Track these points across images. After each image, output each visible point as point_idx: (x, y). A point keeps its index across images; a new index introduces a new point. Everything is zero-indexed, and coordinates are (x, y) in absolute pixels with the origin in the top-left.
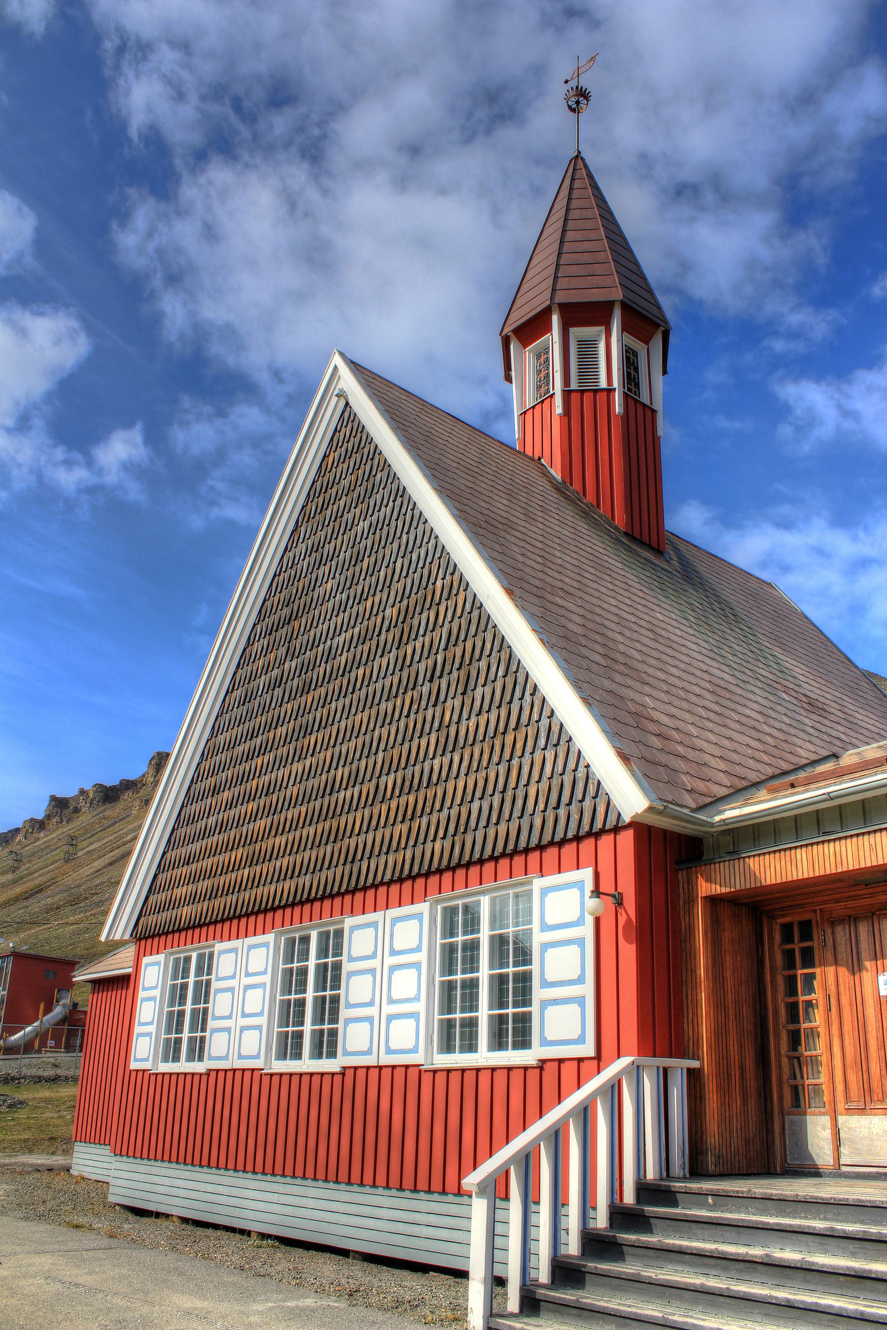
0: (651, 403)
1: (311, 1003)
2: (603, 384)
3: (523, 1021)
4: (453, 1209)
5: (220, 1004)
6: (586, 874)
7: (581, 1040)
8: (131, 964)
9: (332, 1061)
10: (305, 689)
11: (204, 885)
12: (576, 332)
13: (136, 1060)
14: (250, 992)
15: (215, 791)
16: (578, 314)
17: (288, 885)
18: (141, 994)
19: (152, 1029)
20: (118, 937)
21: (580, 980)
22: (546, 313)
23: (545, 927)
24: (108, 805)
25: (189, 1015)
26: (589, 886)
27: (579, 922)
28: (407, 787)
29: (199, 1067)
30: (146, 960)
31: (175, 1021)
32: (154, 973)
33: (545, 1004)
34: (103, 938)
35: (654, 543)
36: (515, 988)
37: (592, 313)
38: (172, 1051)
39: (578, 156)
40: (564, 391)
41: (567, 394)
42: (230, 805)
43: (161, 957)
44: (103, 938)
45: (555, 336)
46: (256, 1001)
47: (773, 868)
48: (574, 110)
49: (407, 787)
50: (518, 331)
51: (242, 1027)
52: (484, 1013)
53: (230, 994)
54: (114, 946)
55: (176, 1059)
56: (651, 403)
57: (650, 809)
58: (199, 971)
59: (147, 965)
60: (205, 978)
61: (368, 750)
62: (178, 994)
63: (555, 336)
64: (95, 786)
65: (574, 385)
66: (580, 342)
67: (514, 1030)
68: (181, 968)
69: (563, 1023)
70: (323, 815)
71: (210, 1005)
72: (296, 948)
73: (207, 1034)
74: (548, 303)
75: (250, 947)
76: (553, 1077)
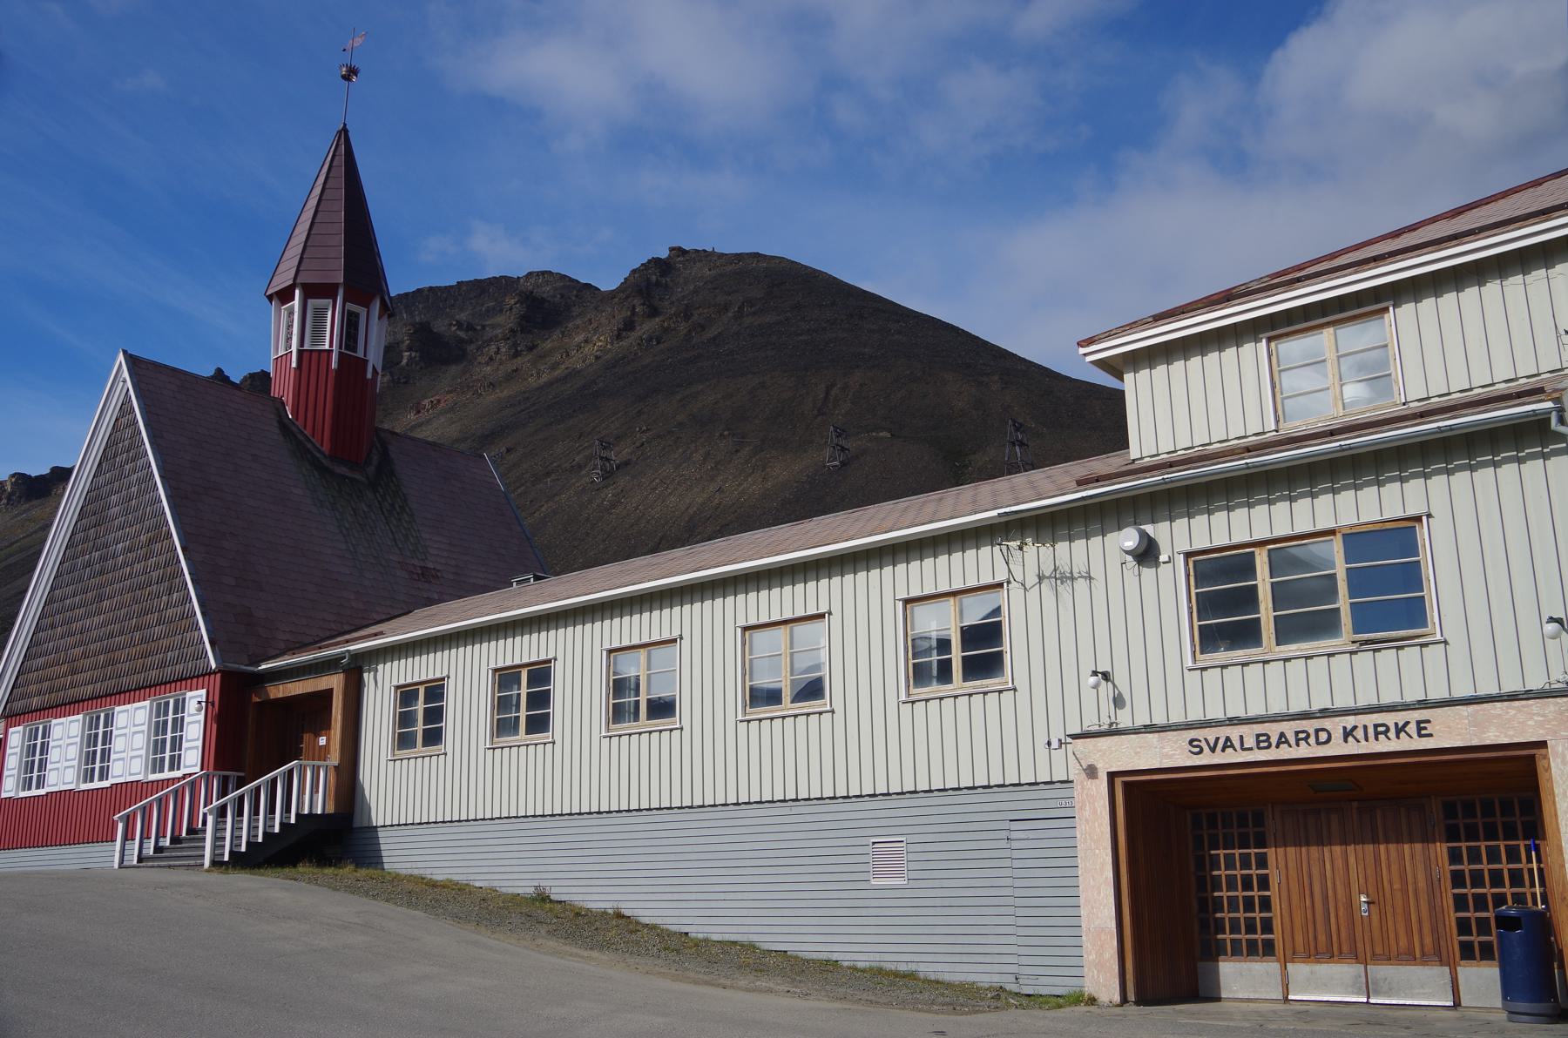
5: (53, 755)
6: (203, 692)
10: (101, 573)
11: (46, 685)
12: (311, 302)
15: (53, 626)
16: (311, 291)
17: (90, 687)
18: (8, 751)
19: (15, 772)
24: (35, 502)
28: (143, 641)
31: (29, 767)
37: (327, 291)
39: (345, 130)
41: (300, 353)
42: (62, 637)
43: (20, 728)
45: (296, 302)
46: (73, 752)
47: (279, 691)
49: (143, 641)
58: (176, 711)
61: (128, 617)
62: (31, 750)
63: (296, 302)
64: (13, 475)
68: (33, 735)
69: (192, 760)
70: (108, 650)
72: (162, 710)
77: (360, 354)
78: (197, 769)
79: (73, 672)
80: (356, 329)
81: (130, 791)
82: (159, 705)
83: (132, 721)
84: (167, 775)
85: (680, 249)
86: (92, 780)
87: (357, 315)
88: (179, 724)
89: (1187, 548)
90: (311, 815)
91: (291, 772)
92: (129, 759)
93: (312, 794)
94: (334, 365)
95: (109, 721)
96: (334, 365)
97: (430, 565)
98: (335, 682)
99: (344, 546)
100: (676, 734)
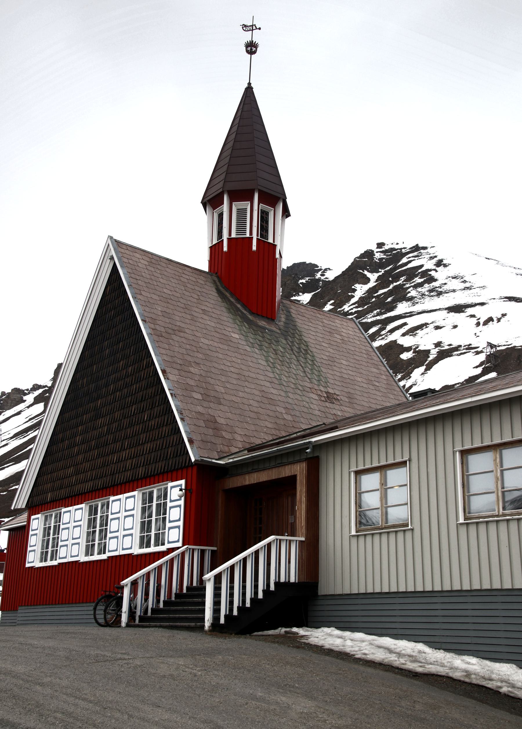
0: (274, 241)
2: (248, 235)
6: (183, 482)
7: (178, 541)
8: (26, 520)
9: (104, 555)
13: (28, 563)
20: (19, 507)
21: (179, 520)
25: (52, 535)
30: (33, 517)
31: (45, 544)
32: (37, 523)
34: (12, 508)
37: (245, 195)
40: (228, 238)
41: (230, 240)
44: (12, 508)
50: (209, 201)
51: (73, 548)
54: (18, 512)
55: (46, 560)
56: (274, 241)
59: (33, 519)
60: (58, 524)
62: (46, 531)
63: (225, 207)
65: (234, 235)
66: (239, 210)
69: (174, 536)
71: (60, 536)
73: (58, 548)
74: (221, 190)
77: (271, 240)
78: (180, 544)
79: (77, 473)
80: (267, 222)
81: (129, 563)
82: (91, 507)
83: (125, 509)
84: (153, 549)
85: (37, 385)
86: (46, 560)
87: (267, 214)
88: (162, 509)
89: (355, 469)
90: (287, 584)
91: (269, 545)
92: (124, 536)
93: (277, 559)
94: (254, 248)
95: (58, 518)
96: (254, 248)
97: (331, 391)
98: (299, 470)
99: (271, 375)
100: (409, 535)
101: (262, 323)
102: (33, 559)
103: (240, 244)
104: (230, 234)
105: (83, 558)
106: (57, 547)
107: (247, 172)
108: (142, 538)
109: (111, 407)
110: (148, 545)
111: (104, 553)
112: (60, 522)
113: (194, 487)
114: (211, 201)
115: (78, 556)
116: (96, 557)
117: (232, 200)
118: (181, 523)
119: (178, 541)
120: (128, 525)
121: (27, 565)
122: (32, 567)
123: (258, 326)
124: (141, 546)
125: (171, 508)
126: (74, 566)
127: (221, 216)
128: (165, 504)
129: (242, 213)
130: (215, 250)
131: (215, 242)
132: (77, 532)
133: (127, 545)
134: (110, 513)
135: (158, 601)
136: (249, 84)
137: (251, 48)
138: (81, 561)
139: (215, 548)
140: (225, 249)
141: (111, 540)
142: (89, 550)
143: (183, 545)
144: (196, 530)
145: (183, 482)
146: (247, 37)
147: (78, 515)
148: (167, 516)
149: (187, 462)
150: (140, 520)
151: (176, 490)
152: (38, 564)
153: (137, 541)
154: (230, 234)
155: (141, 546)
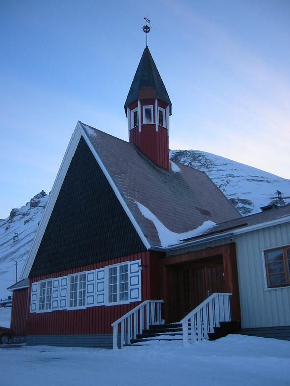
1: (78, 293)
2: (152, 123)
3: (127, 293)
4: (110, 337)
6: (139, 261)
7: (139, 297)
12: (145, 107)
14: (62, 291)
21: (88, 285)
22: (137, 101)
23: (131, 273)
26: (140, 264)
27: (138, 272)
29: (50, 311)
30: (33, 284)
33: (131, 290)
35: (166, 168)
36: (125, 287)
38: (42, 307)
48: (147, 32)
52: (118, 293)
53: (137, 277)
57: (151, 248)
62: (42, 292)
65: (144, 123)
67: (125, 295)
69: (135, 294)
75: (62, 280)
76: (134, 304)
78: (140, 299)
94: (157, 130)
96: (157, 130)
101: (163, 171)
102: (35, 308)
103: (148, 128)
104: (142, 122)
105: (69, 308)
106: (50, 301)
107: (148, 90)
108: (71, 301)
109: (85, 216)
110: (115, 300)
111: (84, 304)
112: (51, 286)
113: (148, 264)
114: (130, 105)
115: (65, 306)
116: (78, 307)
117: (142, 105)
118: (140, 287)
119: (139, 297)
120: (101, 287)
121: (31, 312)
122: (34, 313)
123: (161, 173)
124: (111, 301)
125: (54, 291)
126: (64, 312)
127: (136, 113)
128: (84, 283)
129: (148, 111)
130: (133, 132)
131: (133, 127)
132: (101, 287)
133: (100, 298)
134: (86, 281)
135: (133, 335)
136: (147, 47)
137: (147, 29)
138: (68, 310)
139: (231, 294)
140: (140, 130)
141: (132, 291)
142: (73, 303)
143: (143, 300)
144: (151, 289)
145: (139, 261)
146: (144, 24)
147: (101, 275)
148: (86, 289)
149: (142, 248)
150: (39, 296)
151: (135, 267)
152: (38, 311)
153: (38, 306)
154: (142, 122)
155: (111, 301)
